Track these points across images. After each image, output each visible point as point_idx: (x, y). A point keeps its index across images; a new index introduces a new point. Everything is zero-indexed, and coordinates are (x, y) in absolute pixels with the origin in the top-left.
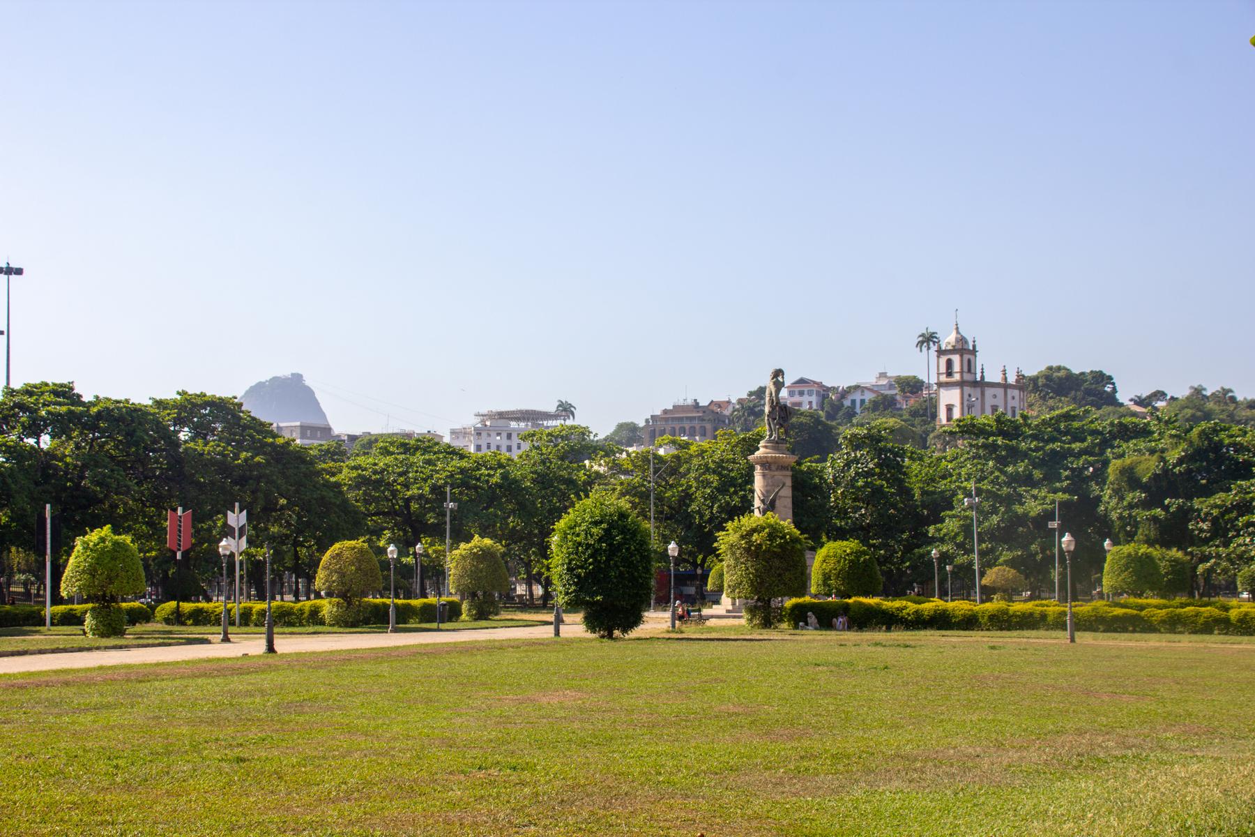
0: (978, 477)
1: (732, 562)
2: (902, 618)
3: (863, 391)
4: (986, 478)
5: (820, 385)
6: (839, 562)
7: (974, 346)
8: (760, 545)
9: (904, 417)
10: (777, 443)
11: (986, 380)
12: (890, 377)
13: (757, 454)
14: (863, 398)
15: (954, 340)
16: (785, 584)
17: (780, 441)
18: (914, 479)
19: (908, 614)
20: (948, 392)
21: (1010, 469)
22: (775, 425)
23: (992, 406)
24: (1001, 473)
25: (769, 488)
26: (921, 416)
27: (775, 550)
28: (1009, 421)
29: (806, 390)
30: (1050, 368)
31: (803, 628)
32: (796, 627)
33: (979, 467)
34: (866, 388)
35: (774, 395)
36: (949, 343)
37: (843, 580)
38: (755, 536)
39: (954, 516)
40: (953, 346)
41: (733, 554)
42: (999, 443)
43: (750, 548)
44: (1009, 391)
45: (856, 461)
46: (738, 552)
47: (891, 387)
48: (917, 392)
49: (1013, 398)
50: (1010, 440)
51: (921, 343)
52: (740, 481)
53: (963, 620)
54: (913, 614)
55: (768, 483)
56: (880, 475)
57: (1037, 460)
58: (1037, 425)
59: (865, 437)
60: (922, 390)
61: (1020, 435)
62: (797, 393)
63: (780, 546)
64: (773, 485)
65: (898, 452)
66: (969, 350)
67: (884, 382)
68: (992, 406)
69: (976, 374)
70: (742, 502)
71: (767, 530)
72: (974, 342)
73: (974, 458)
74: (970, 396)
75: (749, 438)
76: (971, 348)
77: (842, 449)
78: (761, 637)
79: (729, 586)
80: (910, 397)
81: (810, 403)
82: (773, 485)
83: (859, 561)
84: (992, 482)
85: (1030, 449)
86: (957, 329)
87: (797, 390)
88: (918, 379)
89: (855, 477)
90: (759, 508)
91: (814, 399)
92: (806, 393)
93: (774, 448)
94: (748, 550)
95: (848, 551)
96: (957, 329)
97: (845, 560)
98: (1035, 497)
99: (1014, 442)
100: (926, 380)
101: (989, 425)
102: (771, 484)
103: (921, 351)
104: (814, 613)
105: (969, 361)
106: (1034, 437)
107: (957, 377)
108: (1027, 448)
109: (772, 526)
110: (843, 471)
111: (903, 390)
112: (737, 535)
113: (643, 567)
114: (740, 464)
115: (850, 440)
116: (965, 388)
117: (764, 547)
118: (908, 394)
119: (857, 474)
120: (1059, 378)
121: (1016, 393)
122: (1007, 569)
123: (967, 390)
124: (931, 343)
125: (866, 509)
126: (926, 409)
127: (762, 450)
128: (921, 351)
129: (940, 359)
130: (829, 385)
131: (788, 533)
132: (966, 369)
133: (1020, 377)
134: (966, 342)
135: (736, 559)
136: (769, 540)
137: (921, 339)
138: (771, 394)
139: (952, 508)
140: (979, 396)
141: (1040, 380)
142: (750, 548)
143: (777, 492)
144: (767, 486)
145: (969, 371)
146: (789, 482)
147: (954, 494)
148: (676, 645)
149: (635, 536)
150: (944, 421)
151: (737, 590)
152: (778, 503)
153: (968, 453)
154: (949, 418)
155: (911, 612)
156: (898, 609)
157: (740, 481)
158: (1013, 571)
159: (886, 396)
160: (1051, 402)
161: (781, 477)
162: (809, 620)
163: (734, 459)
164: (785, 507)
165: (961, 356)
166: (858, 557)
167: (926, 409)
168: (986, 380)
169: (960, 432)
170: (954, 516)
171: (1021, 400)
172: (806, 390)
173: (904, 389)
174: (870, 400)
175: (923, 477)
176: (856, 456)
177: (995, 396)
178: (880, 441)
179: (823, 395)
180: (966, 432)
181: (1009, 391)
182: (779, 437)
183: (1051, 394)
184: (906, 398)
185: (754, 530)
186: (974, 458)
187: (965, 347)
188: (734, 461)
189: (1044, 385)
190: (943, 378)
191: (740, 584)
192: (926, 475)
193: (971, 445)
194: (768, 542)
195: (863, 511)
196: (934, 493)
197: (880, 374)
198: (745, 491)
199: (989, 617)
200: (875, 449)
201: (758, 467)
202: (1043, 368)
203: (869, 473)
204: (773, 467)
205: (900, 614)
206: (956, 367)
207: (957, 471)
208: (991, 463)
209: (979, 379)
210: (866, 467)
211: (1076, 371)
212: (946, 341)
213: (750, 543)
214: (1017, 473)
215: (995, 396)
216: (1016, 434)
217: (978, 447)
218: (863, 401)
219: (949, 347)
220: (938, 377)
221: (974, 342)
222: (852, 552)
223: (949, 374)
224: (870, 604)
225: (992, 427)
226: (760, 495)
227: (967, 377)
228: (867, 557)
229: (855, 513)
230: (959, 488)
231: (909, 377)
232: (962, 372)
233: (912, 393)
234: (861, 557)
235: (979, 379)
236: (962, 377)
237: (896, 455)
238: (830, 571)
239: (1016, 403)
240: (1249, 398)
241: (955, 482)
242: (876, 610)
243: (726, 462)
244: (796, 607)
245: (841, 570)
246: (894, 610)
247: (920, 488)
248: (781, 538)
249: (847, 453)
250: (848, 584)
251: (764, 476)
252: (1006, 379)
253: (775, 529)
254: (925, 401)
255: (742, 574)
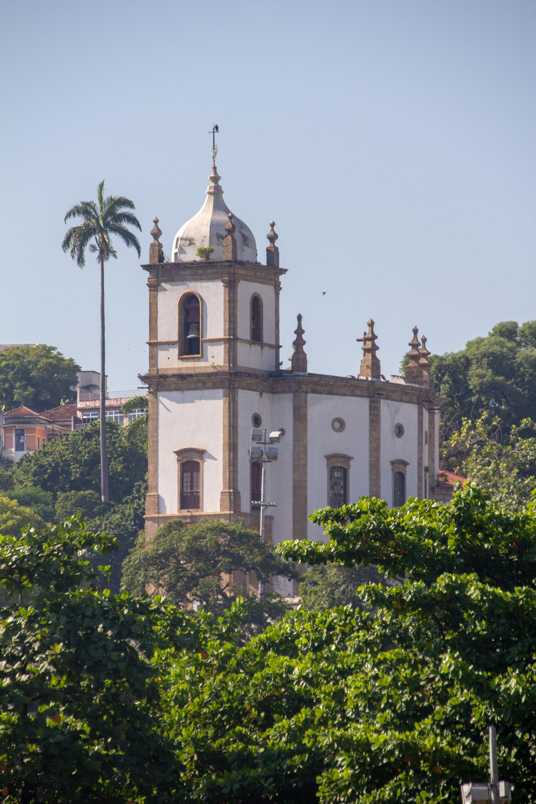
0: (400, 706)
4: (428, 711)
9: (19, 490)
11: (311, 369)
15: (206, 230)
18: (175, 713)
23: (329, 458)
24: (478, 693)
26: (76, 486)
28: (501, 521)
33: (405, 672)
36: (191, 242)
40: (202, 252)
42: (473, 593)
44: (385, 407)
48: (53, 404)
49: (399, 431)
60: (74, 396)
65: (130, 621)
69: (277, 347)
72: (273, 238)
74: (257, 420)
76: (262, 259)
80: (30, 421)
88: (59, 359)
101: (432, 534)
116: (243, 395)
118: (25, 409)
126: (94, 461)
128: (81, 261)
129: (161, 296)
137: (79, 221)
140: (289, 425)
141: (474, 370)
153: (366, 626)
167: (94, 461)
168: (311, 369)
180: (360, 555)
181: (385, 407)
187: (244, 256)
192: (216, 696)
200: (55, 609)
207: (330, 687)
209: (286, 365)
210: (23, 671)
212: (180, 234)
220: (153, 358)
221: (273, 238)
225: (444, 540)
231: (27, 349)
235: (286, 365)
240: (533, 320)
247: (196, 742)
252: (375, 365)
254: (88, 436)
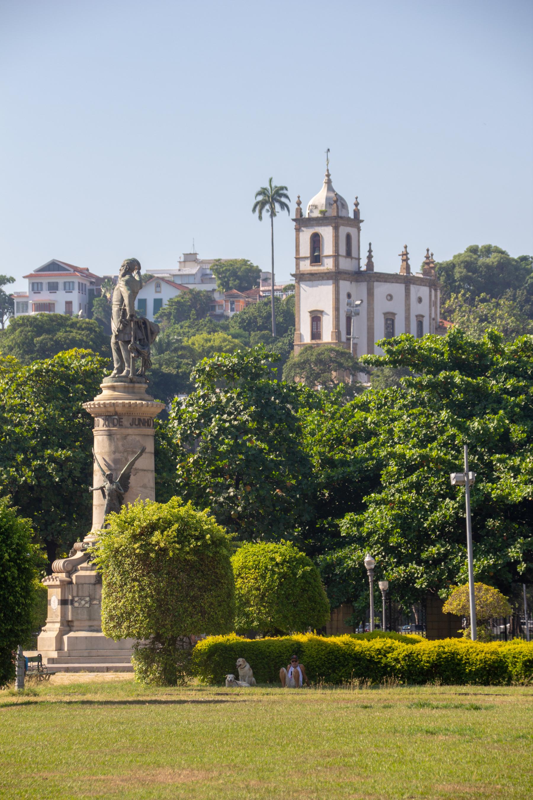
1: (117, 578)
2: (386, 665)
3: (158, 286)
4: (434, 439)
5: (85, 273)
6: (263, 577)
7: (357, 213)
8: (164, 550)
9: (232, 331)
10: (131, 381)
11: (377, 269)
12: (202, 262)
13: (98, 399)
14: (158, 296)
15: (323, 201)
16: (203, 613)
17: (136, 379)
19: (397, 660)
20: (315, 289)
21: (475, 424)
22: (128, 352)
23: (385, 314)
24: (459, 429)
25: (118, 456)
26: (260, 329)
27: (188, 557)
28: (473, 345)
29: (61, 281)
30: (474, 250)
31: (231, 684)
32: (218, 681)
33: (423, 419)
34: (163, 279)
35: (126, 301)
36: (316, 207)
37: (271, 604)
38: (156, 536)
39: (384, 502)
40: (322, 212)
41: (119, 564)
42: (457, 380)
43: (147, 554)
44: (413, 288)
45: (219, 408)
46: (128, 561)
47: (204, 278)
48: (249, 288)
49: (420, 300)
50: (474, 377)
51: (263, 204)
52: (33, 442)
53: (484, 668)
54: (404, 659)
55: (116, 448)
56: (260, 433)
57: (517, 410)
58: (515, 352)
59: (234, 369)
61: (487, 368)
62: (45, 287)
63: (196, 551)
64: (126, 451)
65: (287, 395)
66: (349, 218)
67: (192, 269)
68: (385, 314)
69: (359, 259)
70: (37, 477)
71: (176, 526)
72: (357, 205)
73: (414, 405)
74: (349, 296)
75: (48, 371)
76: (351, 215)
77: (195, 390)
78: (170, 698)
79: (111, 618)
80: (237, 297)
81: (69, 304)
82: (126, 451)
83: (295, 574)
84: (445, 444)
85: (505, 391)
86: (329, 182)
87: (45, 281)
88: (251, 266)
89: (218, 436)
90: (102, 489)
91: (75, 297)
92: (61, 286)
93: (126, 390)
94: (144, 559)
95: (279, 559)
96: (329, 182)
97: (274, 572)
98: (516, 471)
99: (480, 380)
100: (265, 268)
101: (436, 351)
102: (121, 448)
103: (260, 218)
104: (247, 660)
105: (348, 237)
106: (511, 371)
107: (328, 265)
108: (501, 389)
109: (182, 519)
110: (198, 426)
111: (225, 285)
112: (128, 533)
113: (22, 589)
114: (32, 413)
115: (209, 375)
116: (342, 283)
117: (171, 554)
119: (222, 430)
120: (488, 267)
121: (424, 291)
122: (485, 586)
123: (345, 286)
124: (277, 206)
125: (237, 487)
126: (269, 316)
127: (106, 393)
128: (260, 218)
129: (301, 234)
130: (101, 275)
131: (209, 531)
132: (343, 251)
133: (428, 262)
134: (344, 205)
135: (123, 574)
136: (178, 543)
137: (260, 198)
138: (122, 300)
139: (377, 487)
141: (457, 270)
142: (147, 554)
143: (133, 463)
144: (114, 452)
145: (349, 254)
146: (150, 447)
147: (381, 464)
148: (79, 711)
149: (8, 537)
150: (307, 339)
151: (126, 624)
152: (133, 480)
153: (403, 397)
154: (316, 334)
155: (401, 656)
156: (379, 651)
157: (33, 442)
158: (493, 590)
159: (199, 292)
160: (482, 308)
161: (138, 438)
162: (241, 672)
163: (23, 405)
164: (144, 486)
165: (336, 229)
166: (293, 570)
167: (269, 316)
168: (377, 269)
169: (391, 362)
170: (384, 502)
171: (432, 304)
172: (61, 281)
173: (227, 283)
174: (171, 300)
175: (323, 436)
176: (219, 402)
177: (390, 297)
178: (257, 376)
179: (91, 291)
180: (400, 362)
181: (413, 288)
182: (135, 371)
183: (482, 295)
184: (232, 299)
185: (153, 527)
186: (414, 405)
187: (342, 214)
188: (22, 409)
189: (464, 279)
190: (306, 266)
191: (130, 614)
192: (329, 431)
193: (410, 385)
194: (177, 546)
195: (232, 492)
196: (344, 463)
197: (186, 255)
198: (42, 458)
199: (525, 663)
200: (251, 389)
201: (100, 422)
202: (462, 250)
203: (242, 429)
204: (126, 422)
205: (384, 661)
206: (328, 248)
208: (444, 414)
209: (363, 268)
210: (235, 419)
211: (514, 254)
212: (311, 203)
213: (147, 547)
214: (486, 429)
215: (390, 297)
216: (479, 366)
217: (419, 387)
218: (158, 303)
219: (316, 214)
220: (298, 265)
221: (357, 205)
222: (284, 561)
223: (316, 259)
224: (335, 644)
225: (442, 354)
226: (105, 468)
227: (346, 264)
228: (308, 568)
229: (218, 494)
230: (392, 455)
231: (235, 261)
232: (336, 256)
233: (241, 289)
234: (298, 569)
235: (363, 268)
236: (336, 264)
237: (285, 399)
238: (248, 592)
239: (423, 309)
241: (383, 444)
242: (344, 655)
243: (9, 411)
244: (215, 649)
245: (266, 590)
246: (373, 654)
248: (197, 539)
249: (203, 397)
250: (278, 612)
251: (110, 435)
252: (408, 268)
253: (186, 524)
254: (266, 304)
255: (133, 597)
